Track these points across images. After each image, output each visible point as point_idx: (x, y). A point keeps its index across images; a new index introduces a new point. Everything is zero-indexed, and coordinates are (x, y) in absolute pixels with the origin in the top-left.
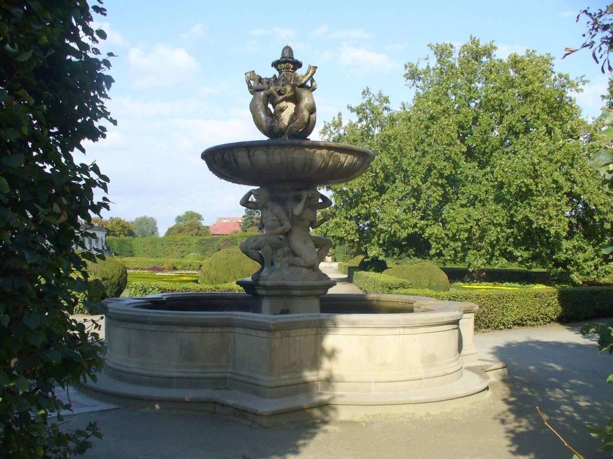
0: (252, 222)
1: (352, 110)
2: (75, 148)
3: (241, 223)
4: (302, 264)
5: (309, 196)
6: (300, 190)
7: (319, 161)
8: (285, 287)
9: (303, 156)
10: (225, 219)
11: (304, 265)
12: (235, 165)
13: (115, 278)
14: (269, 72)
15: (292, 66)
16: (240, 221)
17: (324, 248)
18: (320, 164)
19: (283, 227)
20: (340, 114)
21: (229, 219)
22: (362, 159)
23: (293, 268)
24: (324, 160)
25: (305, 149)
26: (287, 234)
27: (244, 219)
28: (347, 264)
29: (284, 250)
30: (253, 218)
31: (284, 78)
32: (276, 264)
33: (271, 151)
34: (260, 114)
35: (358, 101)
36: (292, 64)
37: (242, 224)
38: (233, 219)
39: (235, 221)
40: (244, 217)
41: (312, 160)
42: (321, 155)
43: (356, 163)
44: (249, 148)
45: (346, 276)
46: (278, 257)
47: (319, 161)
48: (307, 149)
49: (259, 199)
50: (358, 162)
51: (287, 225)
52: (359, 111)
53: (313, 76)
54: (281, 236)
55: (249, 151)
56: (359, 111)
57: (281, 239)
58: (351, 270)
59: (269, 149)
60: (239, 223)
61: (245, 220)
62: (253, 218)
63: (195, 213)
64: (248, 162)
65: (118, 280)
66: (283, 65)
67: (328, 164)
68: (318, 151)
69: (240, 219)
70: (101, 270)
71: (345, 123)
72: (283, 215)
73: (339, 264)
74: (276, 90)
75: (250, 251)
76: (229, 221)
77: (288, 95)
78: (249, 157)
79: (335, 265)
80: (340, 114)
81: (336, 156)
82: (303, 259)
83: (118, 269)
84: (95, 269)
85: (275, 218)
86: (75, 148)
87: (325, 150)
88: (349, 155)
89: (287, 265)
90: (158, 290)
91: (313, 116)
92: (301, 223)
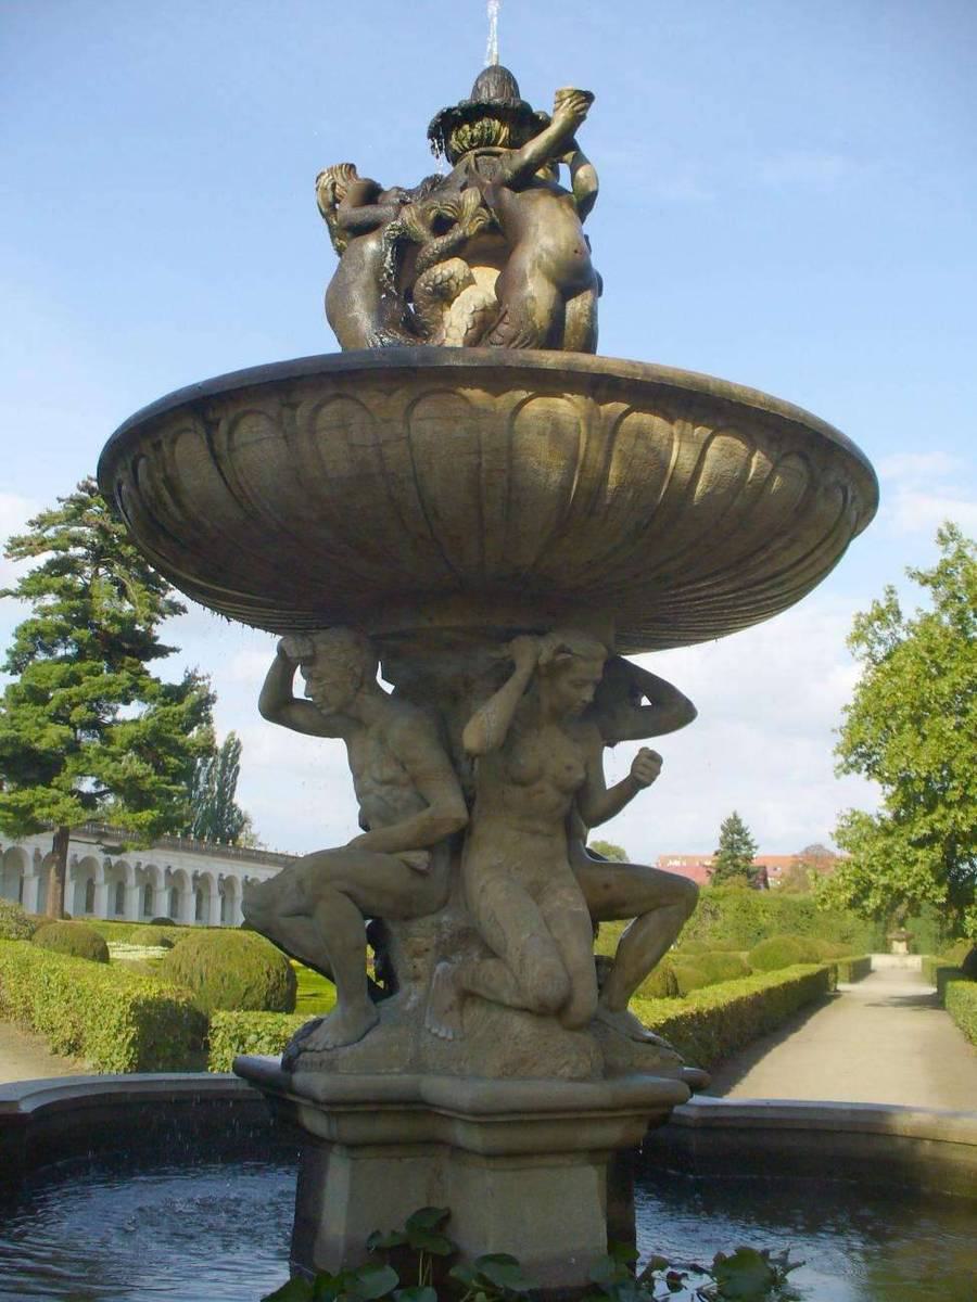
0: (734, 866)
1: (925, 581)
2: (608, 787)
3: (711, 867)
4: (507, 997)
5: (543, 660)
6: (508, 636)
7: (544, 465)
8: (414, 1106)
9: (459, 430)
10: (674, 858)
11: (517, 1001)
12: (173, 508)
13: (255, 991)
14: (407, 162)
15: (505, 132)
16: (708, 863)
17: (654, 918)
18: (556, 477)
19: (426, 813)
20: (892, 592)
21: (684, 858)
22: (794, 463)
23: (475, 1013)
24: (575, 459)
25: (468, 392)
26: (457, 843)
27: (717, 858)
28: (941, 960)
29: (439, 926)
30: (736, 857)
31: (466, 177)
32: (405, 986)
33: (302, 412)
34: (355, 321)
35: (932, 558)
36: (503, 124)
37: (713, 871)
38: (693, 858)
39: (697, 864)
40: (716, 854)
41: (510, 451)
42: (556, 429)
43: (762, 486)
44: (211, 416)
45: (933, 990)
46: (417, 954)
47: (544, 465)
48: (476, 395)
49: (319, 679)
50: (777, 481)
51: (448, 803)
52: (937, 579)
53: (578, 136)
54: (420, 858)
55: (211, 426)
56: (937, 579)
57: (416, 872)
58: (944, 975)
59: (294, 406)
60: (707, 867)
61: (720, 861)
62: (736, 857)
63: (610, 847)
64: (217, 483)
65: (266, 998)
66: (467, 127)
67: (604, 478)
68: (537, 406)
69: (708, 858)
70: (219, 971)
71: (909, 614)
72: (428, 755)
73: (923, 961)
74: (422, 217)
75: (285, 922)
76: (684, 864)
77: (467, 228)
78: (216, 457)
79: (915, 962)
80: (892, 592)
81: (641, 434)
82: (511, 970)
83: (265, 969)
84: (205, 968)
85: (390, 771)
86: (608, 787)
87: (577, 399)
88: (717, 432)
89: (450, 997)
90: (271, 1043)
91: (575, 306)
92: (517, 794)
